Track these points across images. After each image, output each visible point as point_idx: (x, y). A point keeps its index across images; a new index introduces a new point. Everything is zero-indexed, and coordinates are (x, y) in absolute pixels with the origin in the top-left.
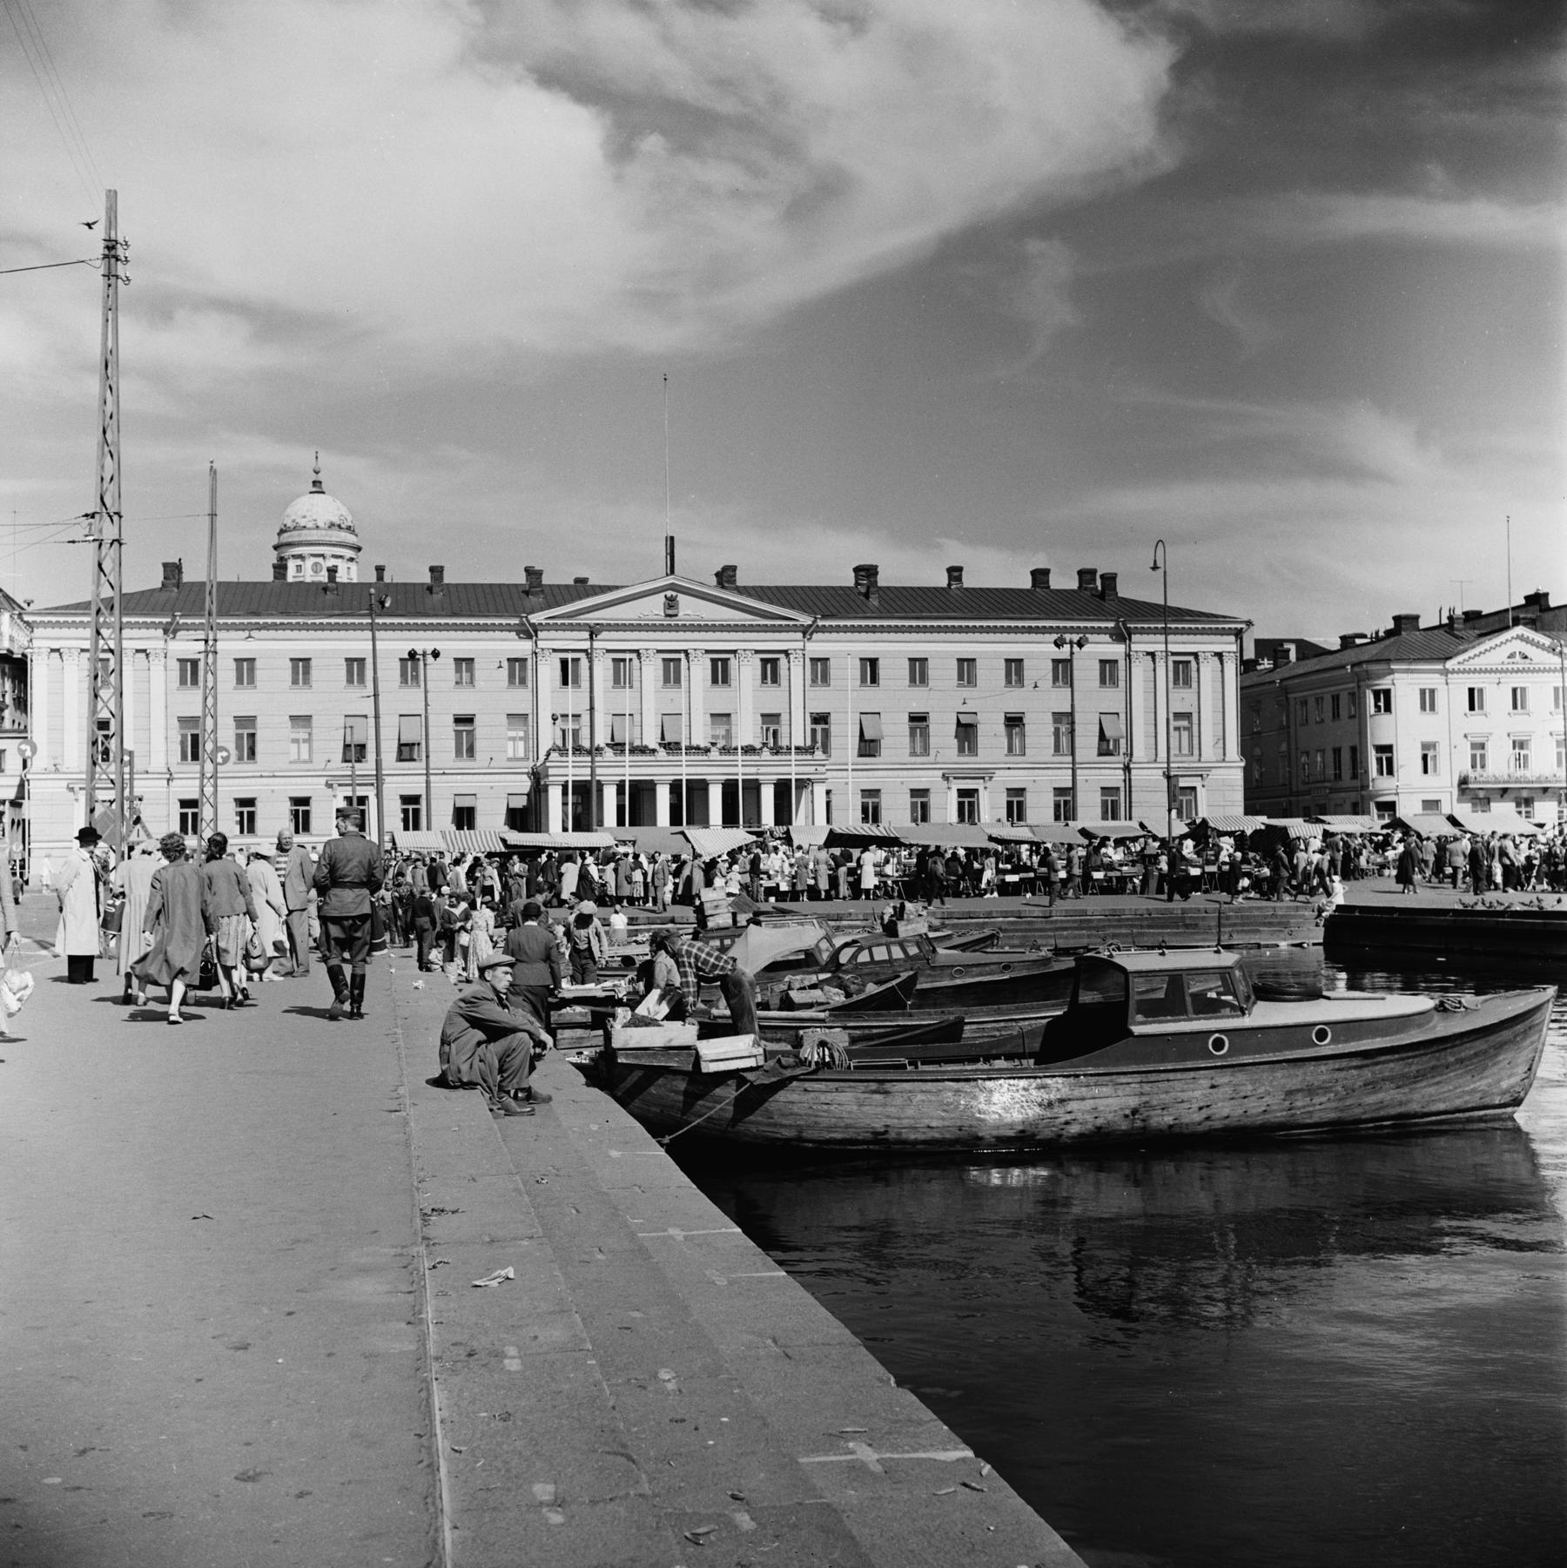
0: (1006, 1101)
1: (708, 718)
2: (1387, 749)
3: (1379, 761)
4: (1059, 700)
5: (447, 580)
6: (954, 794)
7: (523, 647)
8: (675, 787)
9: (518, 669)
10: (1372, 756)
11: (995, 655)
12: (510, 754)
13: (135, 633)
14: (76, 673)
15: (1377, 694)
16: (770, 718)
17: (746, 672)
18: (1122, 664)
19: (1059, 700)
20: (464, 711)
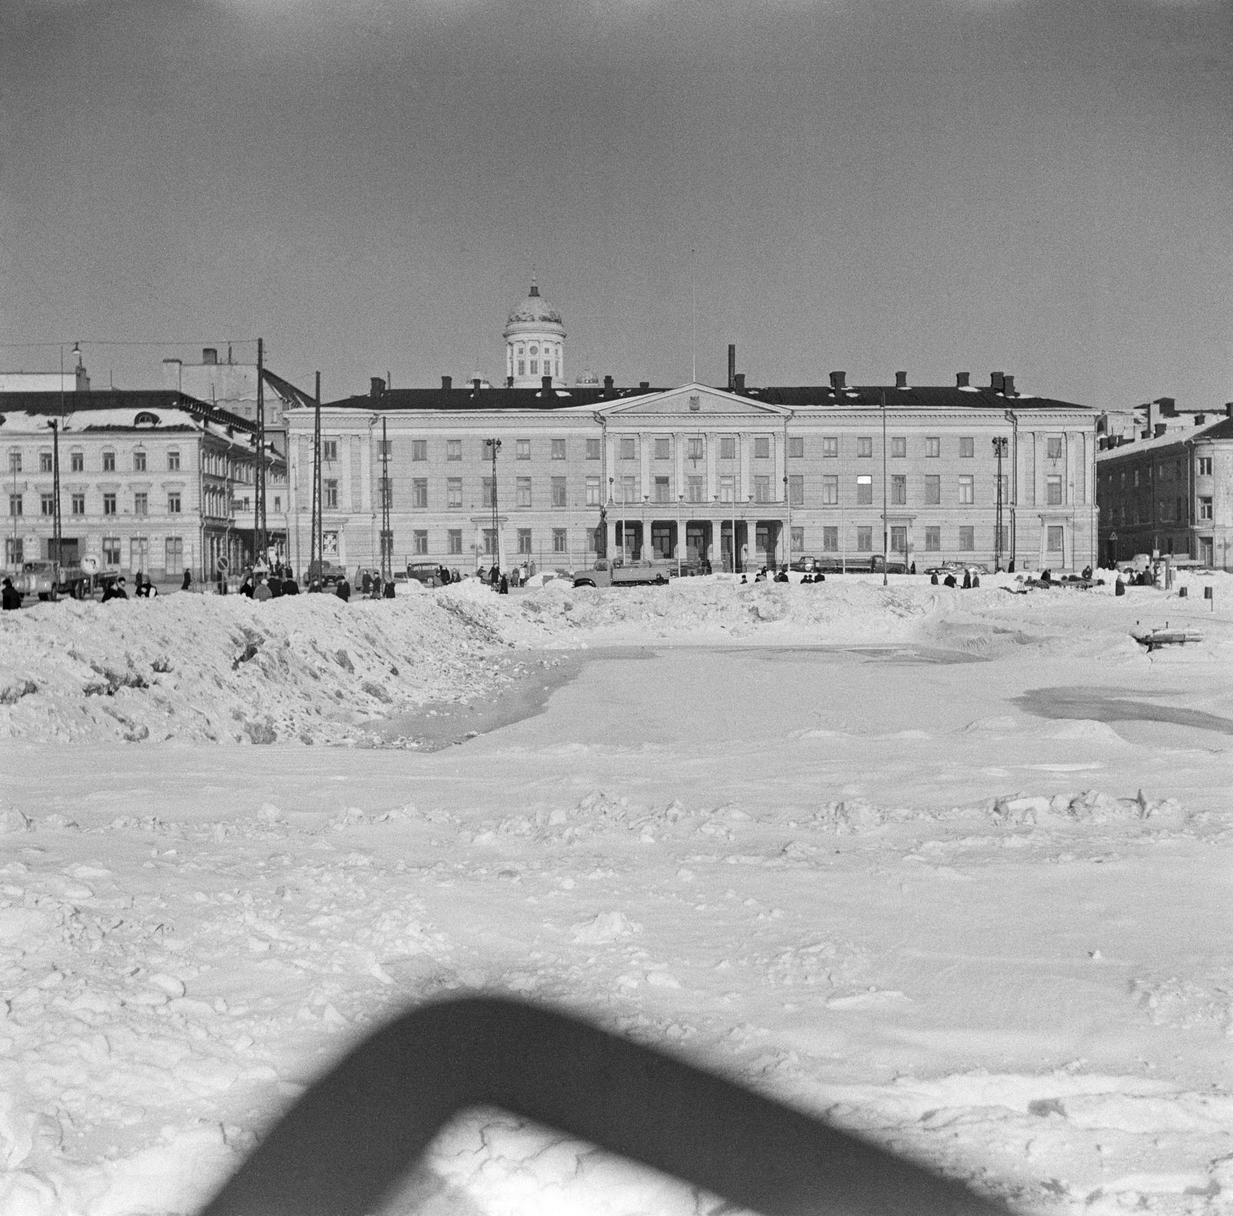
0: (340, 778)
1: (654, 480)
2: (1208, 500)
3: (1203, 508)
4: (486, 469)
5: (453, 387)
6: (1046, 530)
7: (595, 431)
8: (726, 525)
9: (594, 448)
10: (1199, 504)
11: (580, 436)
12: (590, 502)
13: (894, 421)
14: (367, 453)
15: (1202, 460)
16: (662, 481)
17: (745, 450)
18: (1010, 441)
19: (486, 469)
20: (663, 474)
